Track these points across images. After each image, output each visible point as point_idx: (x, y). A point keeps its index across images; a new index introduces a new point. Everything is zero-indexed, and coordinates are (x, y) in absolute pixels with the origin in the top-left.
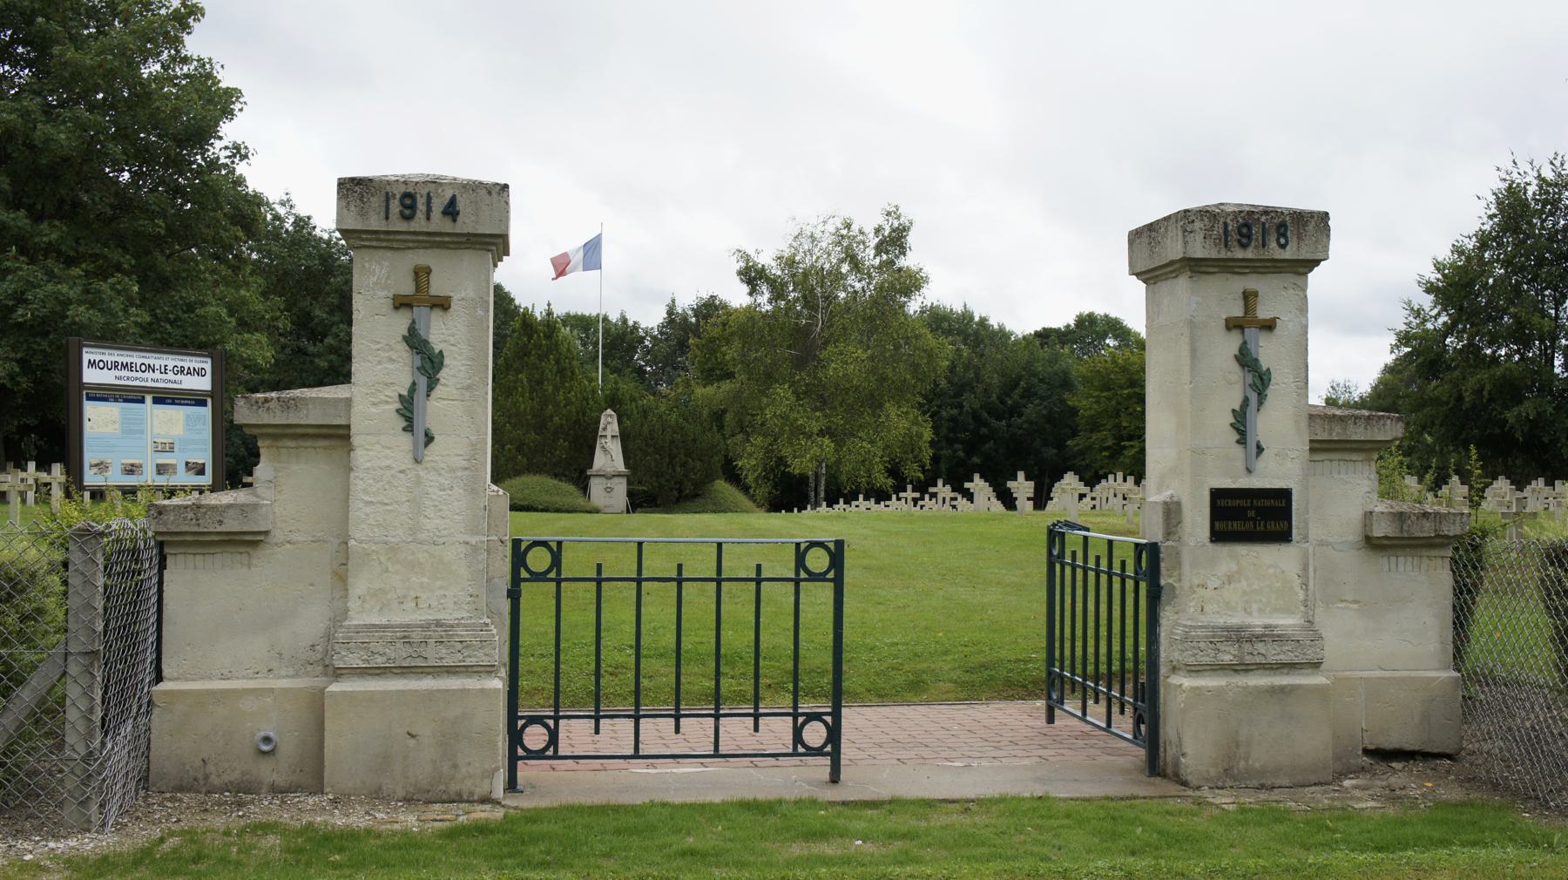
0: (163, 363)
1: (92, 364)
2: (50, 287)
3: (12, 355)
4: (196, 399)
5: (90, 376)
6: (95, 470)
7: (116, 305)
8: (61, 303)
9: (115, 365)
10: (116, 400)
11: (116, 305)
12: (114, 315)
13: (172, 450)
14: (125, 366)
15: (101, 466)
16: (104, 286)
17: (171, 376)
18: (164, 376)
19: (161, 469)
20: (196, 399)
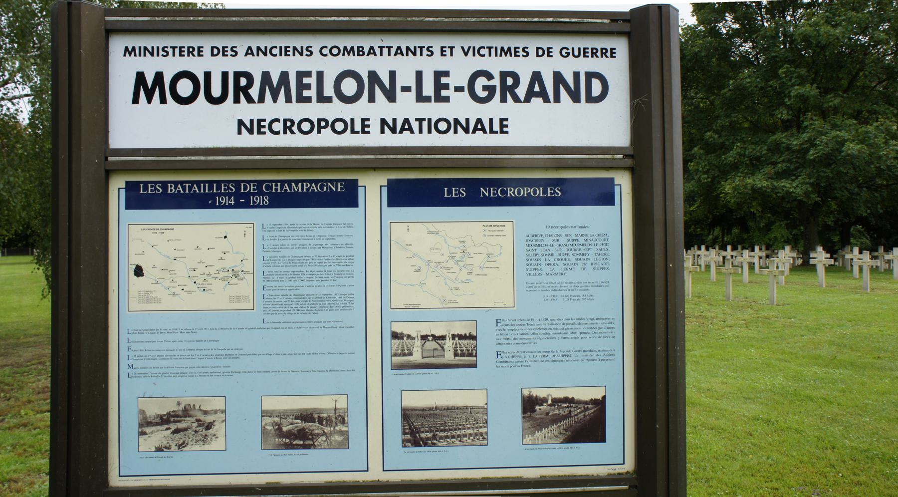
0: (429, 65)
1: (146, 88)
2: (834, 133)
3: (807, 180)
4: (565, 181)
5: (136, 126)
6: (160, 436)
7: (880, 140)
8: (837, 142)
9: (240, 87)
10: (242, 201)
11: (880, 140)
12: (878, 147)
13: (466, 358)
14: (274, 87)
15: (183, 423)
16: (870, 128)
17: (460, 106)
18: (433, 111)
19: (420, 428)
20: (565, 181)
